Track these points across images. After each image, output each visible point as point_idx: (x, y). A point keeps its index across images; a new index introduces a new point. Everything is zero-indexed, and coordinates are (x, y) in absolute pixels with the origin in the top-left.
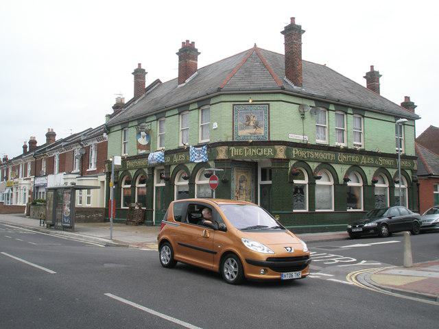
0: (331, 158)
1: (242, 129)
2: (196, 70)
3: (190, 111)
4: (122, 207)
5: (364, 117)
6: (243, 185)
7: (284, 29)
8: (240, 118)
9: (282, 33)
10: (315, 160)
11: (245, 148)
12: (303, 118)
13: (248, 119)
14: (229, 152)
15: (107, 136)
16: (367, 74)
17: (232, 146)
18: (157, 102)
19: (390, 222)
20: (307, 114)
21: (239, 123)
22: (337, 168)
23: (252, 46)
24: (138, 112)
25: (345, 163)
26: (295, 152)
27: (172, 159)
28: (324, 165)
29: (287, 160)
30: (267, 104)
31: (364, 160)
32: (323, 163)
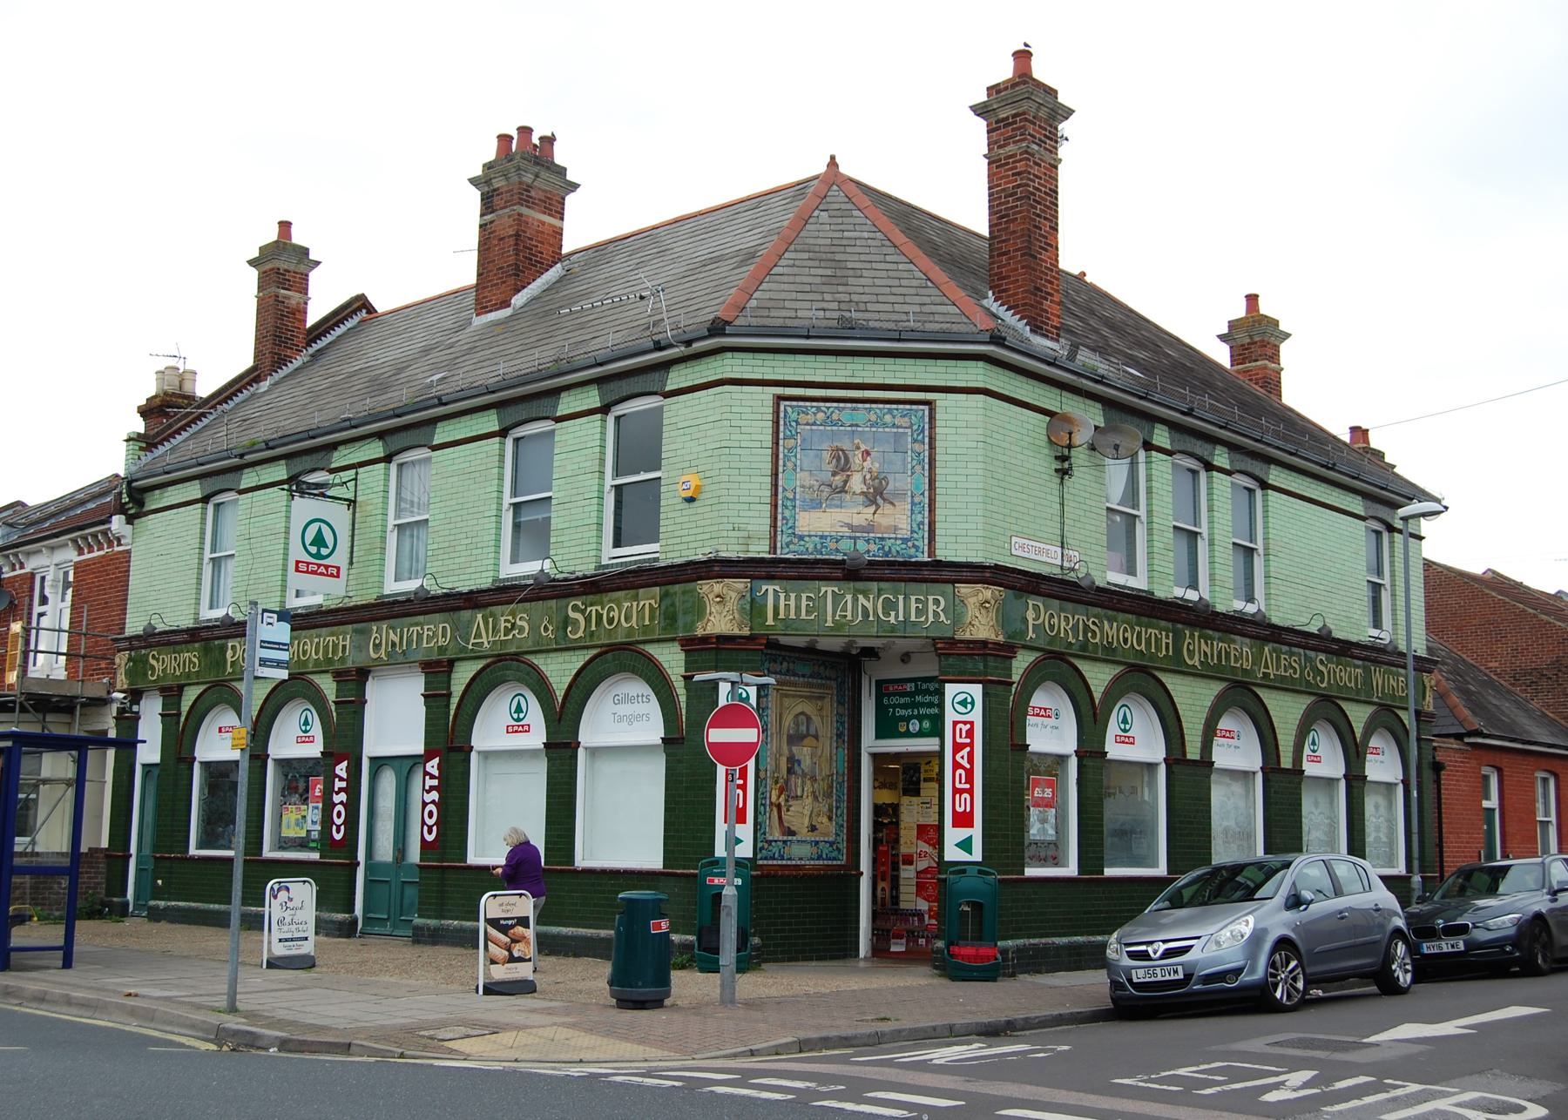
0: (1158, 648)
1: (815, 505)
2: (558, 257)
3: (241, 492)
4: (193, 851)
5: (1264, 485)
6: (804, 753)
7: (256, 254)
8: (804, 459)
9: (253, 263)
10: (1107, 654)
11: (828, 589)
12: (1064, 473)
13: (842, 464)
14: (755, 608)
15: (127, 530)
16: (1233, 325)
17: (770, 578)
18: (379, 385)
19: (1304, 928)
20: (1080, 457)
21: (801, 478)
22: (1179, 687)
23: (821, 168)
24: (290, 422)
25: (1205, 673)
26: (1036, 614)
27: (462, 631)
28: (1137, 675)
29: (1006, 651)
30: (923, 397)
31: (1273, 661)
32: (1133, 668)
